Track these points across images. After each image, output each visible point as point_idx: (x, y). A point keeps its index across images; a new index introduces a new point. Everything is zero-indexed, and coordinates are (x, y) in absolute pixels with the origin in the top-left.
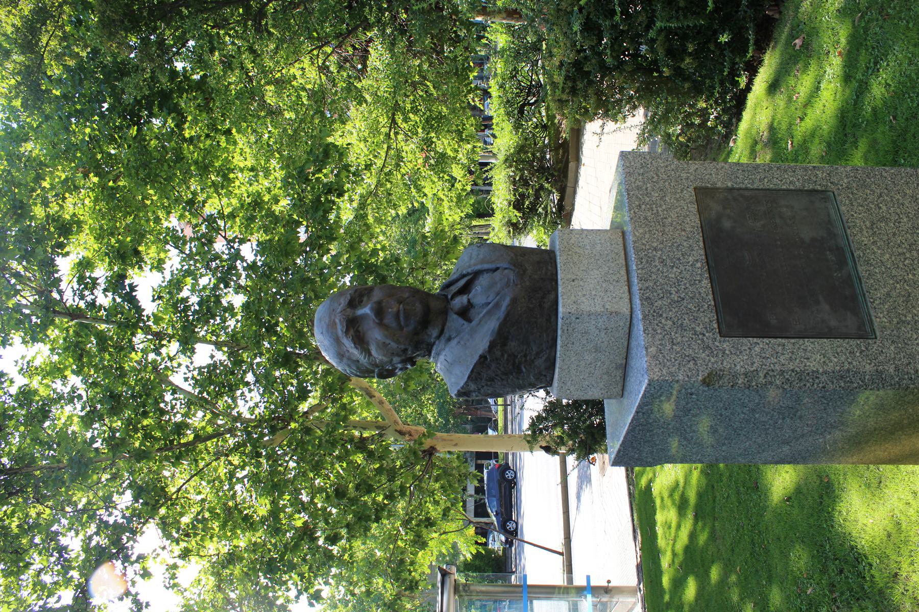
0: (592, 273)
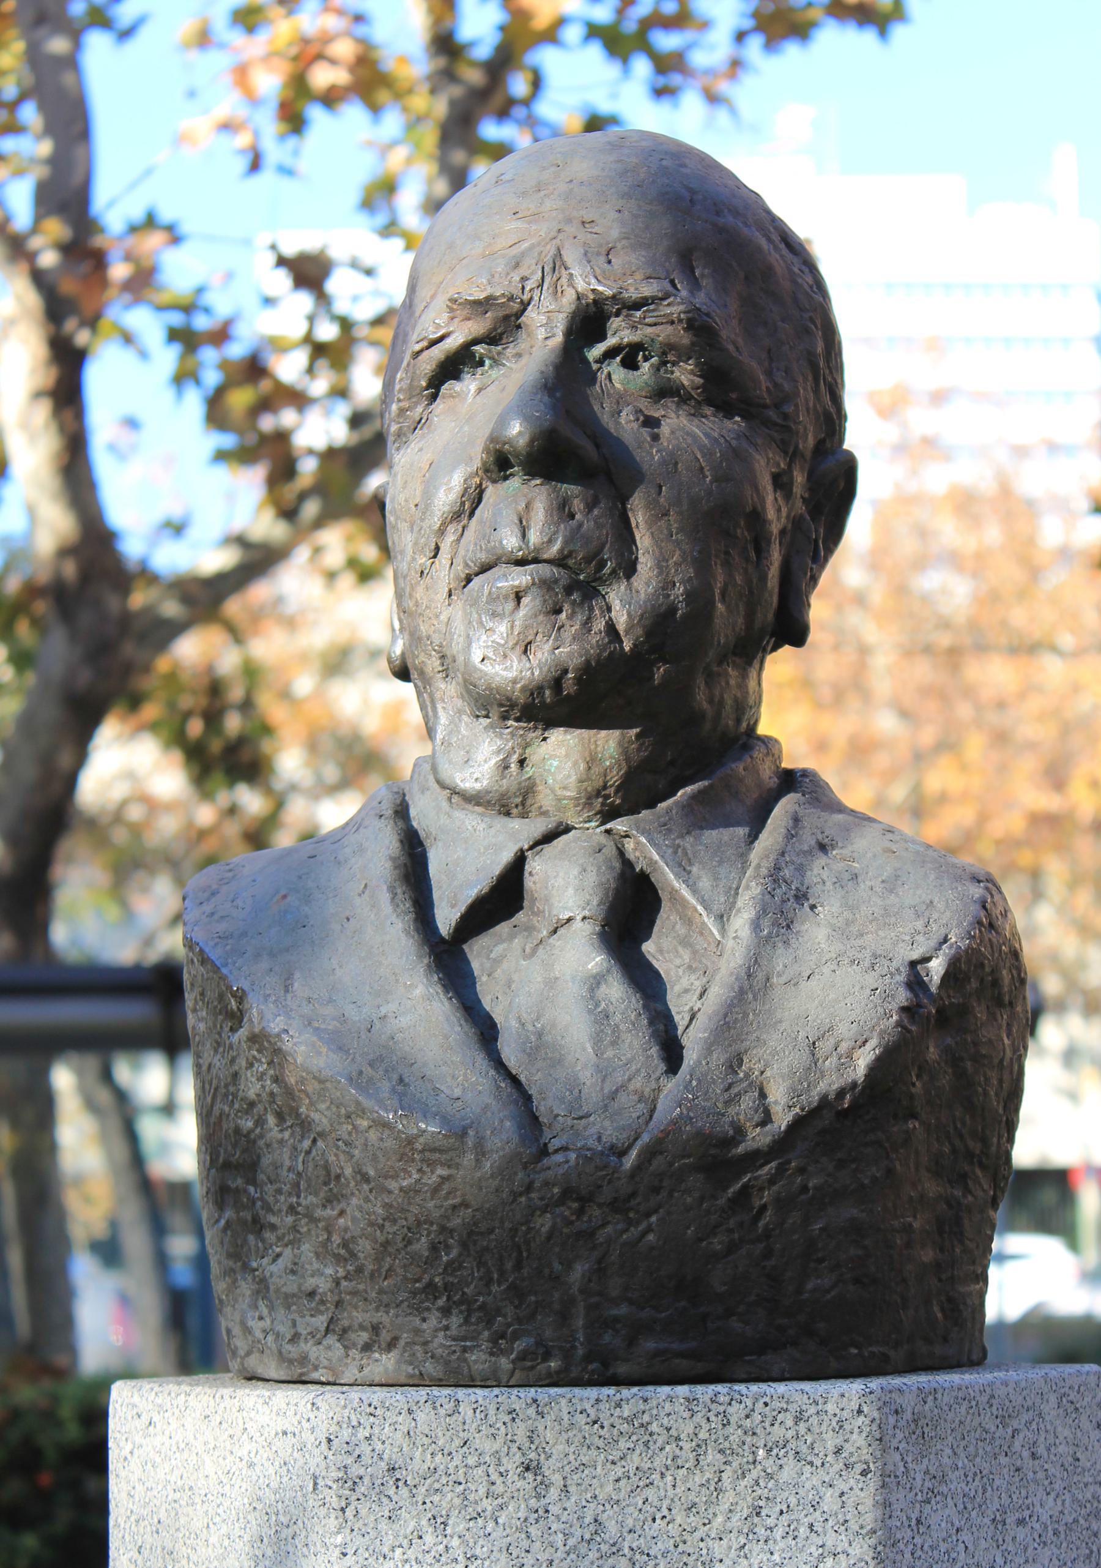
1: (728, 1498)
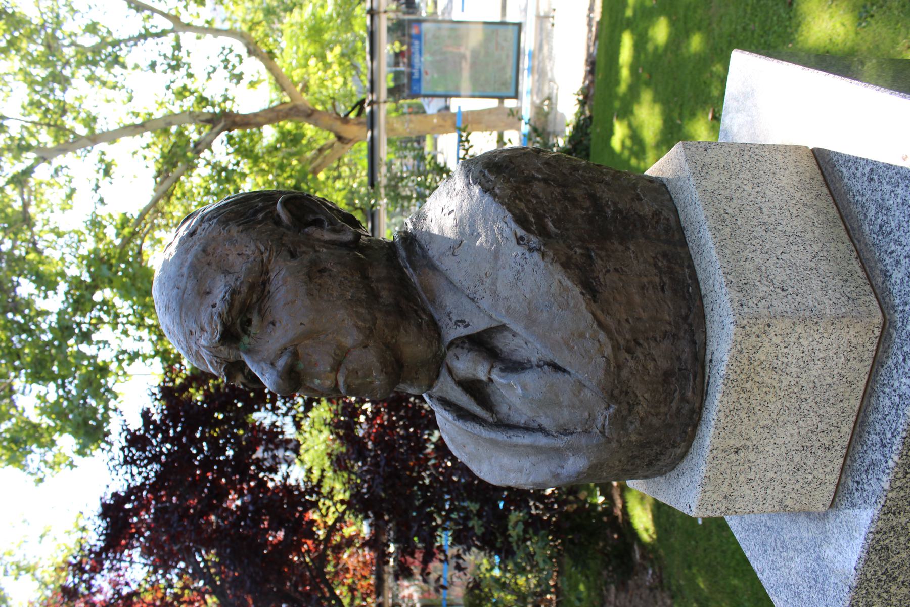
0: (781, 432)
1: (766, 379)
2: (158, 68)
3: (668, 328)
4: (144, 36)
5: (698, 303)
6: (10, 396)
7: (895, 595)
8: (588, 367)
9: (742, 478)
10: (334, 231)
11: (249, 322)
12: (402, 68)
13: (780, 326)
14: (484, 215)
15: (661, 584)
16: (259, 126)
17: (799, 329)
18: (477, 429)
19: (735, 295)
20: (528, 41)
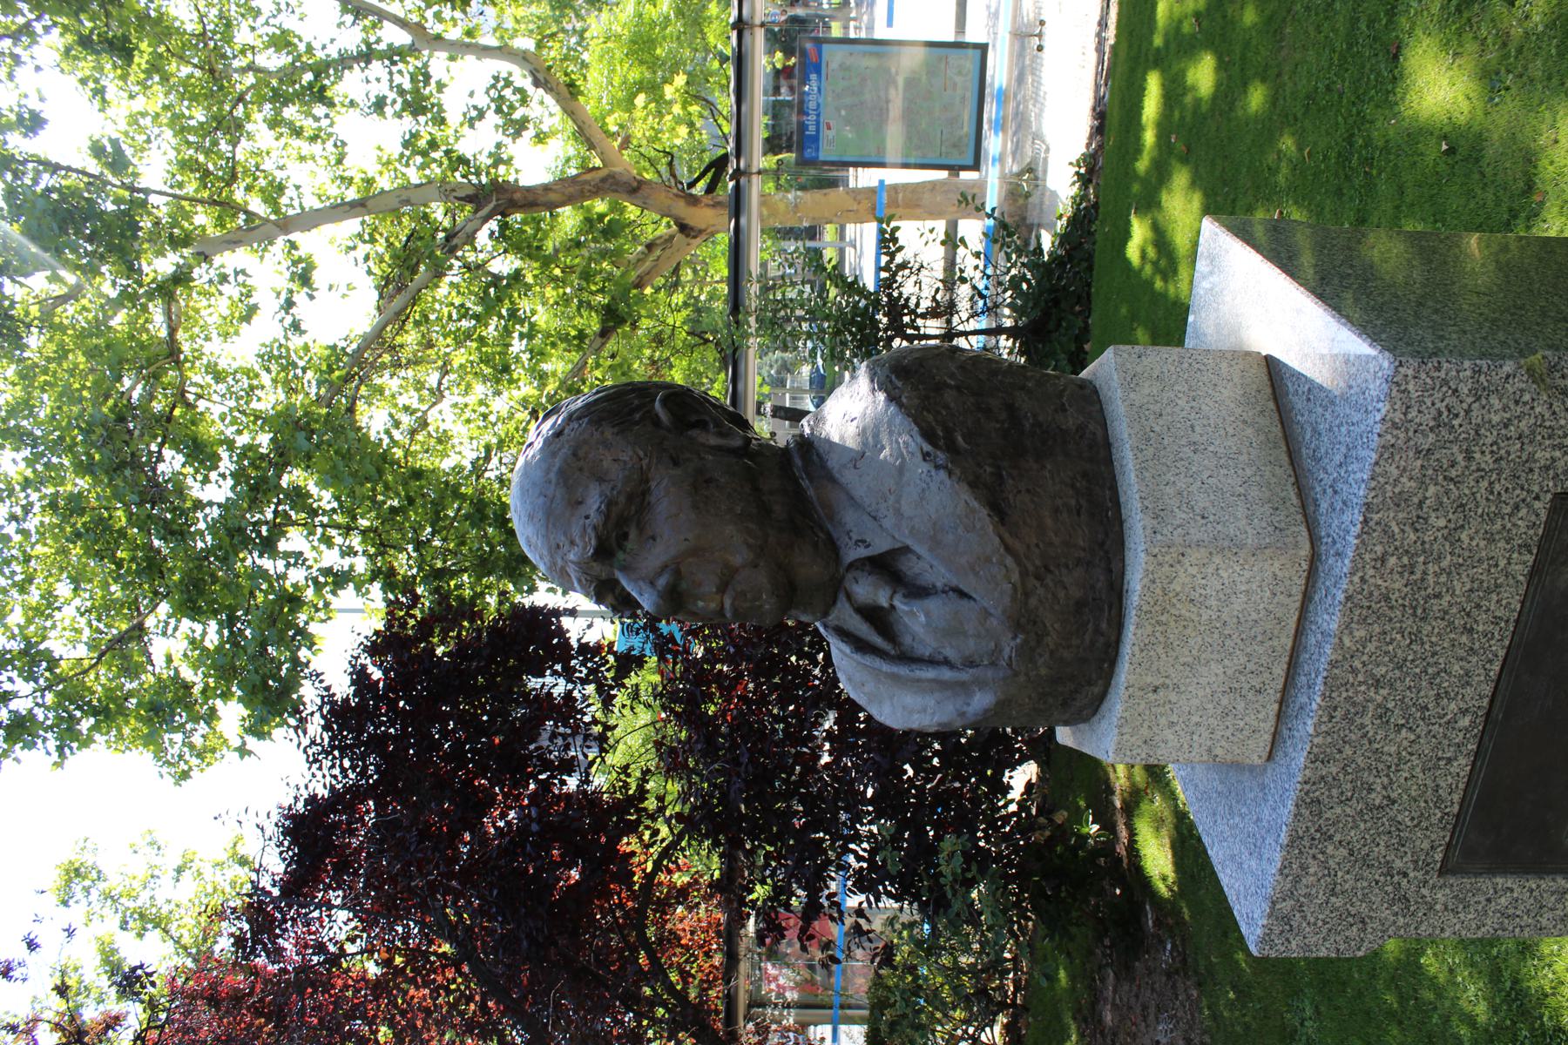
0: (1203, 670)
2: (388, 110)
3: (1082, 554)
4: (367, 56)
5: (1117, 528)
6: (140, 638)
7: (1333, 856)
8: (993, 595)
9: (1163, 721)
10: (721, 435)
11: (625, 536)
12: (785, 95)
13: (1195, 555)
14: (889, 426)
15: (1183, 966)
16: (552, 207)
17: (1217, 559)
18: (877, 663)
19: (1150, 523)
20: (999, 71)
